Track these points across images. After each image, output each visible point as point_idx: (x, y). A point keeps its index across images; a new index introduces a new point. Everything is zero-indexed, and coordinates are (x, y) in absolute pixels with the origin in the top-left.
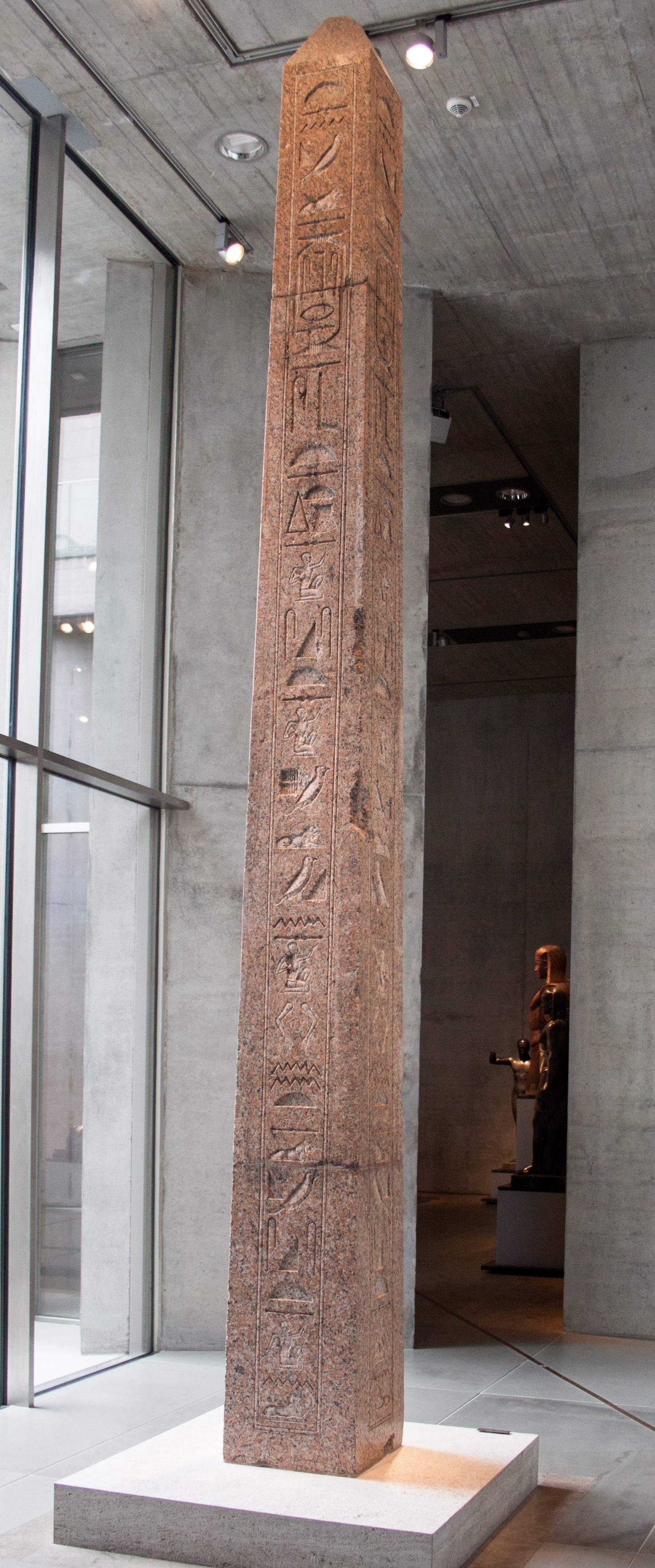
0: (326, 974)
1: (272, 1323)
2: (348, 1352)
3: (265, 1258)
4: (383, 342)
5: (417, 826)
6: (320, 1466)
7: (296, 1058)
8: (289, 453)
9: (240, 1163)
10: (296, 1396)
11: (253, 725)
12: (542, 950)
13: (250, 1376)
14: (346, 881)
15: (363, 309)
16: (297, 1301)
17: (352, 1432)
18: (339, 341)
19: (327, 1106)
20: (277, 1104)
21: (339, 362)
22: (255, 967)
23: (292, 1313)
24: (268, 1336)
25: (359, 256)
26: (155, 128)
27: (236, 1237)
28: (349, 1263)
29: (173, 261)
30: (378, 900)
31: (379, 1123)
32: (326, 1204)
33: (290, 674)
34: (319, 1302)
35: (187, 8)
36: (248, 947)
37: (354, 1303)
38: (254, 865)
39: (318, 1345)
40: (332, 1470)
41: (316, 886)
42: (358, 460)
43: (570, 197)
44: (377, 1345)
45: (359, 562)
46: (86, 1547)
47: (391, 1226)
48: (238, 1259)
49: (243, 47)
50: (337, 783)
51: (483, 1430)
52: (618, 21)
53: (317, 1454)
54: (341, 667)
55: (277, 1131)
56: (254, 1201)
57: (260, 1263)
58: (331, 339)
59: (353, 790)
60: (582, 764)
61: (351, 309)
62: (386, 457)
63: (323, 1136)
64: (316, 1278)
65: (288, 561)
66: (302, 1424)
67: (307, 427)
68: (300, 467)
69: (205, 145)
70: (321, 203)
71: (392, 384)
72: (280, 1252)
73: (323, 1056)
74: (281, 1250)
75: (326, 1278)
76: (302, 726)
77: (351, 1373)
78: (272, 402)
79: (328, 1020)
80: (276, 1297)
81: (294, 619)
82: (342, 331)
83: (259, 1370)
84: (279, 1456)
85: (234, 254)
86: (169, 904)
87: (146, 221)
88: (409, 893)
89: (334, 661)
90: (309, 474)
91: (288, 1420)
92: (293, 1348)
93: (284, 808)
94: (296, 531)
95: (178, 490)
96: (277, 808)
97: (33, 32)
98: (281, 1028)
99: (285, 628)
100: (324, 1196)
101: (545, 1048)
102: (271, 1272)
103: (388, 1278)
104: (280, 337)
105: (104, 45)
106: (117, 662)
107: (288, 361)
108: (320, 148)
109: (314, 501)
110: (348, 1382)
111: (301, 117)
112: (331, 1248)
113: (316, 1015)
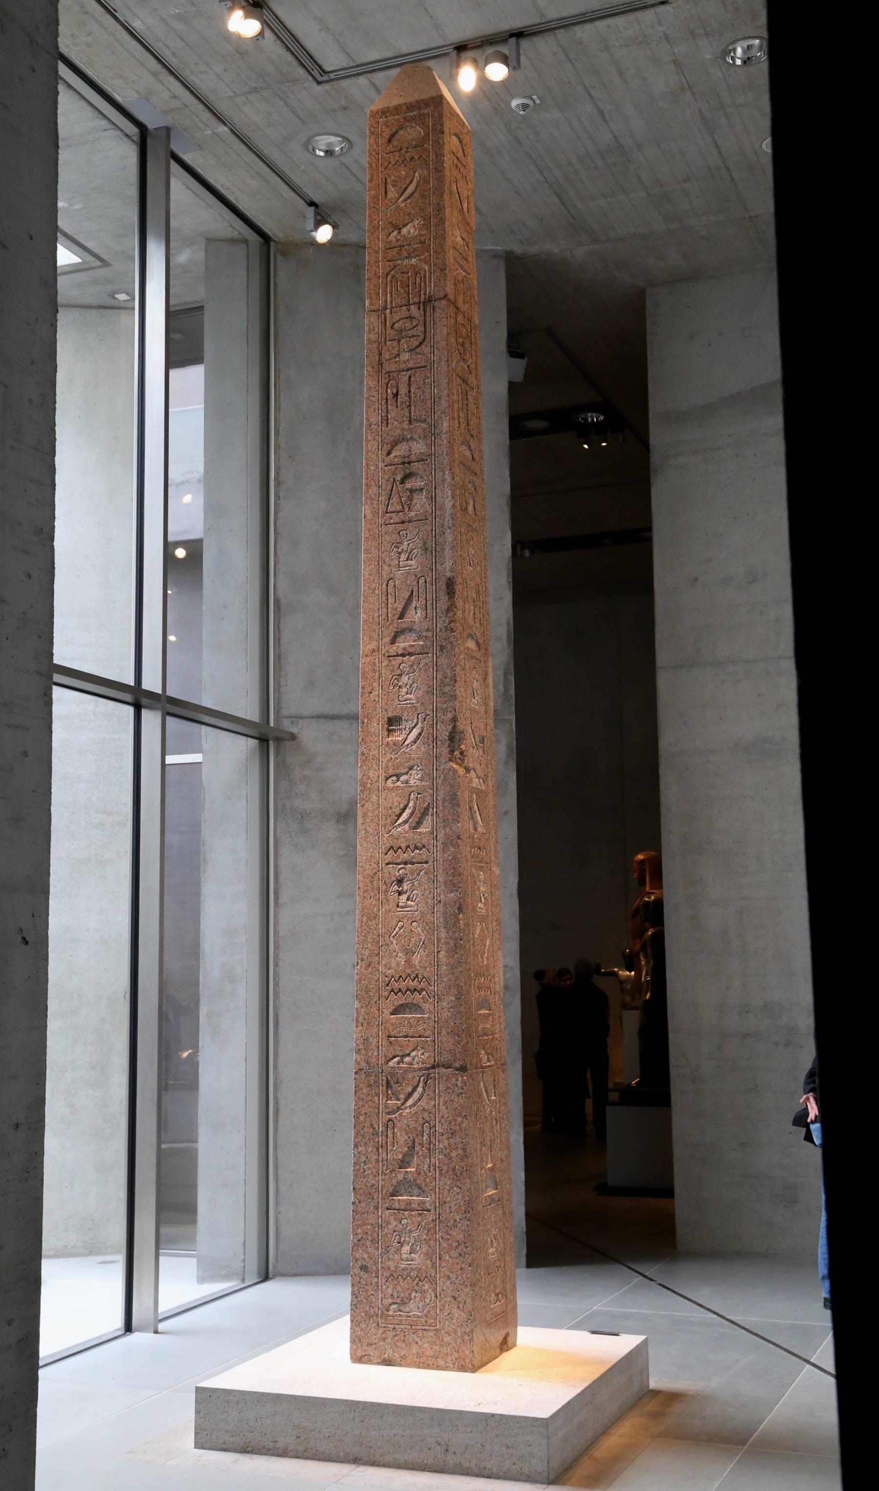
0: (432, 895)
1: (392, 1220)
4: (463, 345)
5: (509, 747)
6: (441, 1362)
7: (408, 971)
8: (385, 445)
9: (361, 1070)
10: (416, 1292)
11: (362, 679)
12: (640, 857)
13: (374, 1274)
14: (447, 812)
16: (415, 1198)
17: (469, 1325)
18: (426, 349)
19: (438, 1013)
20: (392, 1014)
21: (426, 366)
22: (370, 891)
25: (439, 275)
27: (358, 1140)
28: (462, 1160)
30: (475, 829)
32: (439, 1104)
33: (393, 634)
35: (278, 42)
36: (364, 874)
37: (468, 1199)
38: (367, 801)
40: (452, 1366)
46: (225, 1450)
48: (361, 1160)
49: (328, 69)
51: (594, 1332)
52: (661, 29)
53: (438, 1350)
55: (393, 1039)
56: (374, 1105)
57: (380, 1164)
59: (450, 733)
60: (663, 681)
61: (434, 320)
62: (468, 443)
65: (387, 537)
67: (400, 423)
68: (395, 457)
70: (405, 231)
71: (472, 379)
72: (399, 1152)
74: (400, 1150)
75: (441, 1175)
76: (405, 679)
77: (466, 1266)
78: (369, 402)
79: (436, 936)
80: (396, 1196)
81: (395, 587)
82: (427, 340)
83: (382, 1268)
84: (402, 1354)
85: (324, 234)
86: (278, 830)
87: (240, 207)
89: (431, 622)
90: (403, 463)
91: (409, 1317)
92: (413, 1245)
93: (391, 750)
94: (394, 512)
95: (277, 447)
96: (385, 751)
97: (142, 65)
99: (387, 595)
100: (437, 1097)
101: (646, 957)
103: (497, 1175)
104: (374, 346)
105: (205, 72)
106: (225, 607)
107: (382, 366)
108: (403, 183)
109: (408, 486)
110: (464, 1276)
111: (385, 155)
112: (444, 1146)
113: (425, 932)
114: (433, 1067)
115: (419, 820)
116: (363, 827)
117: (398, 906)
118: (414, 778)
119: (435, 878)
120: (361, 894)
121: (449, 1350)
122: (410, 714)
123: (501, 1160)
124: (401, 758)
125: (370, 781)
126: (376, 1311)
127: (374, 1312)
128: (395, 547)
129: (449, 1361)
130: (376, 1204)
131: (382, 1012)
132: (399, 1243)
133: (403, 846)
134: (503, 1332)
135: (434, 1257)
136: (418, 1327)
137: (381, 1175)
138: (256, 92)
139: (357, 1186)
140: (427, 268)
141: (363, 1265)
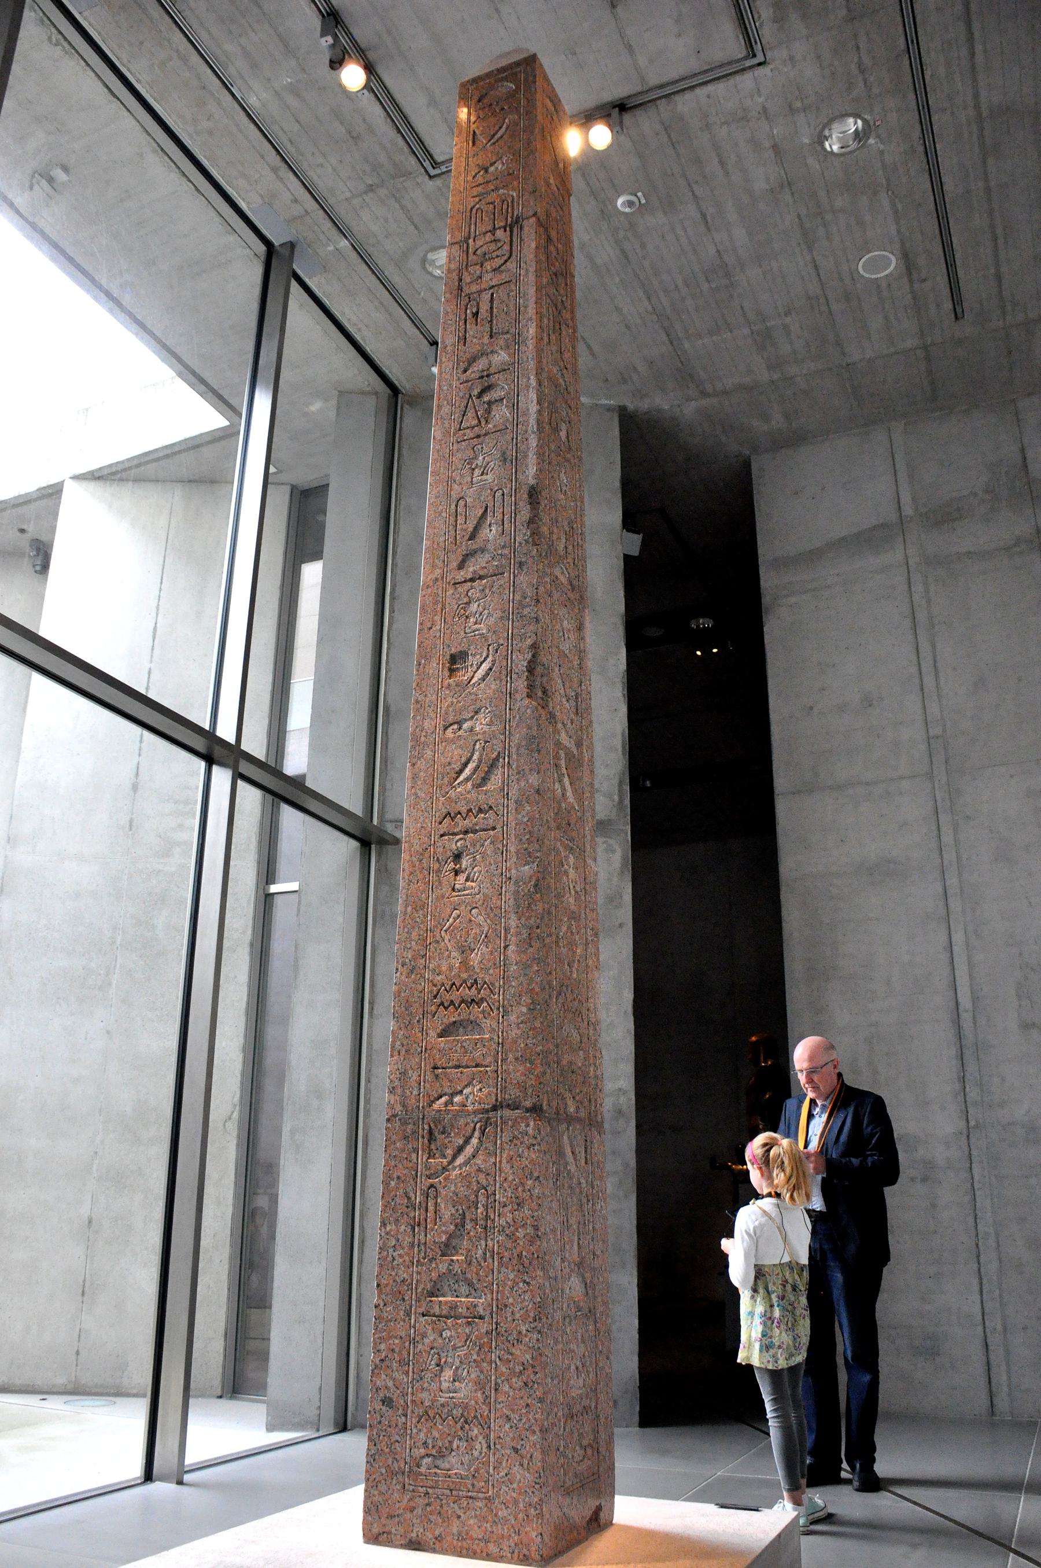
0: (500, 870)
1: (430, 1332)
2: (530, 1370)
3: (423, 1241)
5: (624, 858)
7: (464, 976)
10: (460, 1439)
13: (400, 1412)
14: (522, 761)
15: (533, 236)
16: (463, 1300)
17: (537, 1493)
18: (511, 265)
19: (502, 1033)
20: (440, 1036)
23: (456, 1317)
24: (425, 1351)
26: (370, 250)
27: (386, 1215)
28: (532, 1242)
29: (394, 390)
31: (571, 1063)
32: (500, 1162)
33: (460, 559)
34: (492, 1299)
35: (389, 120)
37: (539, 1300)
38: (419, 759)
39: (491, 1362)
40: (509, 1555)
41: (488, 773)
42: (530, 356)
43: (731, 296)
44: (573, 1367)
45: (533, 442)
47: (590, 1205)
49: (439, 158)
50: (512, 658)
52: (761, 100)
54: (515, 543)
55: (440, 1070)
57: (416, 1249)
58: (502, 265)
59: (529, 662)
63: (497, 1071)
64: (488, 1267)
66: (469, 1482)
69: (414, 263)
73: (497, 970)
74: (444, 1229)
76: (474, 607)
79: (503, 925)
80: (437, 1296)
81: (466, 506)
83: (413, 1401)
84: (437, 1533)
88: (617, 923)
89: (508, 538)
90: (482, 377)
91: (449, 1477)
92: (457, 1368)
96: (445, 694)
98: (446, 941)
99: (456, 516)
102: (430, 1261)
103: (588, 1275)
105: (322, 165)
109: (486, 399)
112: (507, 1222)
113: (488, 921)
114: (494, 1108)
117: (453, 890)
118: (481, 724)
121: (506, 1531)
122: (478, 647)
123: (594, 1254)
126: (402, 1466)
127: (400, 1468)
128: (468, 463)
129: (505, 1548)
130: (408, 1307)
131: (427, 1034)
132: (438, 1365)
133: (464, 810)
134: (593, 1504)
135: (488, 1388)
136: (461, 1493)
137: (417, 1267)
138: (372, 190)
139: (384, 1282)
140: (515, 194)
141: (385, 1397)
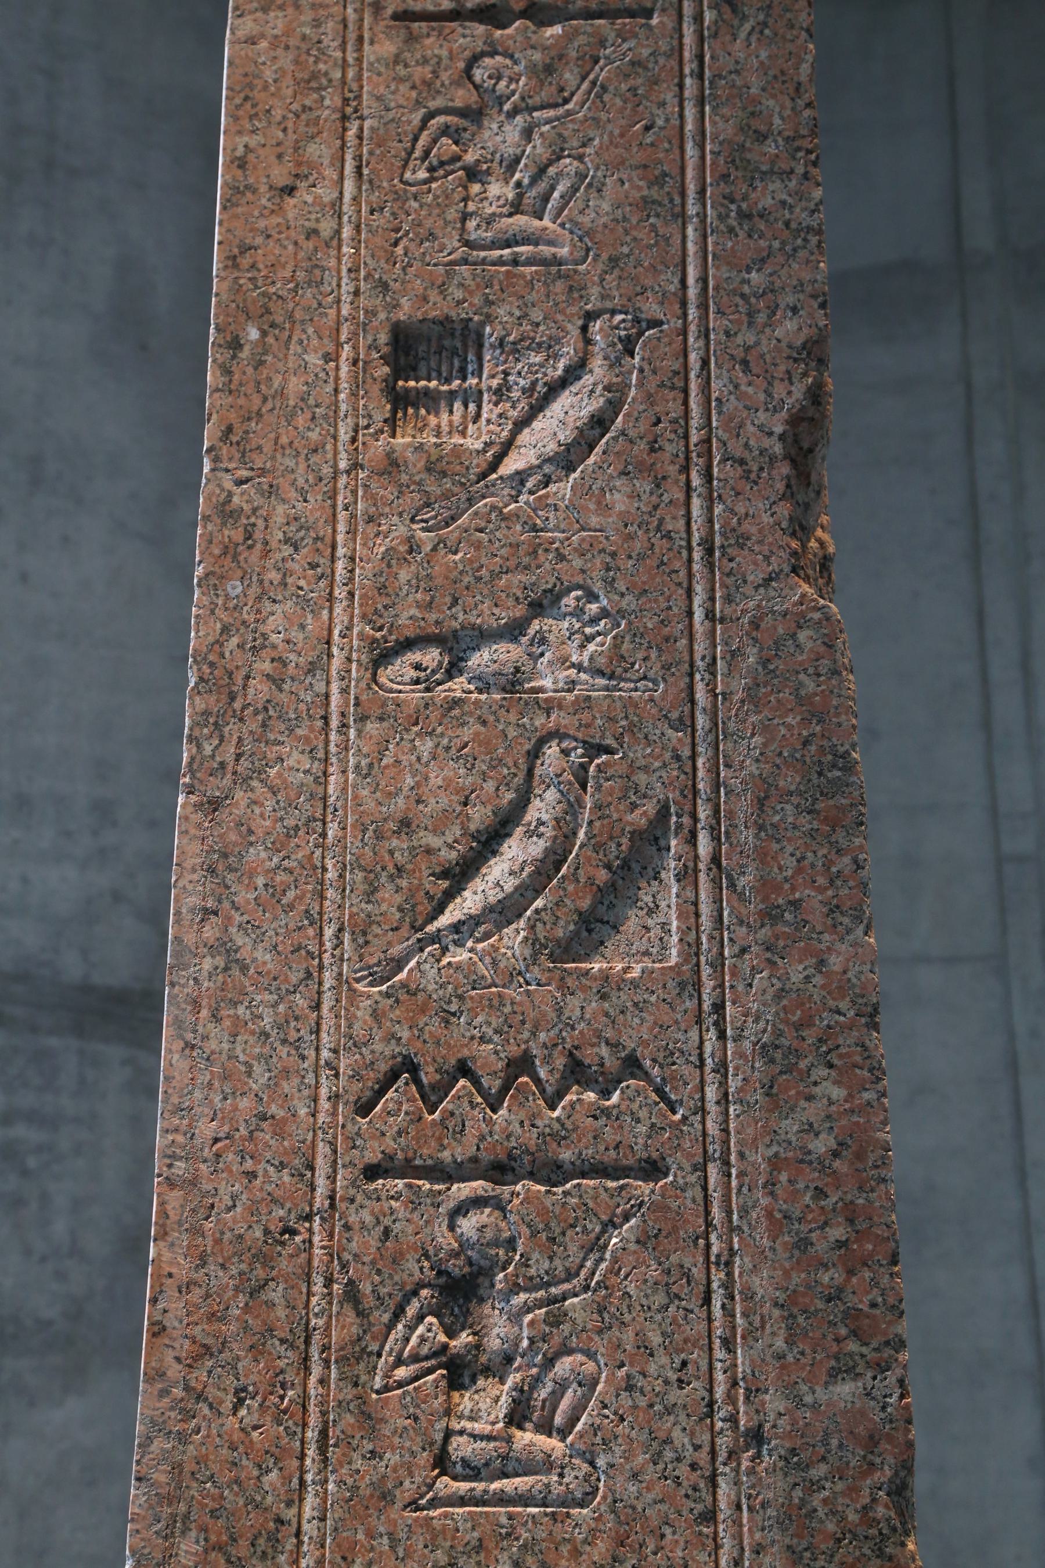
11: (234, 117)
22: (238, 1349)
36: (197, 1231)
59: (795, 420)
96: (371, 498)
115: (598, 902)
116: (210, 932)
117: (442, 1462)
119: (718, 1277)
120: (175, 1371)
122: (537, 315)
124: (478, 546)
125: (267, 666)
